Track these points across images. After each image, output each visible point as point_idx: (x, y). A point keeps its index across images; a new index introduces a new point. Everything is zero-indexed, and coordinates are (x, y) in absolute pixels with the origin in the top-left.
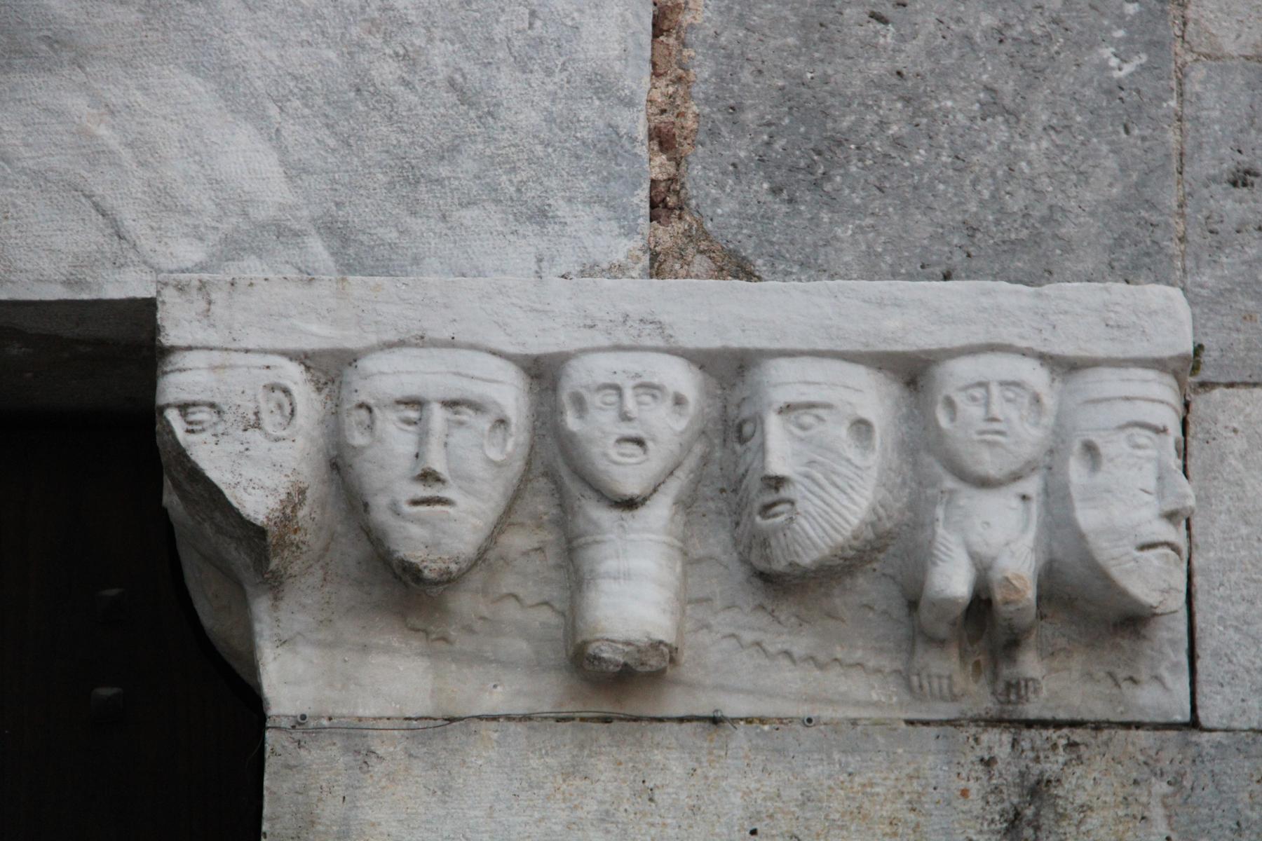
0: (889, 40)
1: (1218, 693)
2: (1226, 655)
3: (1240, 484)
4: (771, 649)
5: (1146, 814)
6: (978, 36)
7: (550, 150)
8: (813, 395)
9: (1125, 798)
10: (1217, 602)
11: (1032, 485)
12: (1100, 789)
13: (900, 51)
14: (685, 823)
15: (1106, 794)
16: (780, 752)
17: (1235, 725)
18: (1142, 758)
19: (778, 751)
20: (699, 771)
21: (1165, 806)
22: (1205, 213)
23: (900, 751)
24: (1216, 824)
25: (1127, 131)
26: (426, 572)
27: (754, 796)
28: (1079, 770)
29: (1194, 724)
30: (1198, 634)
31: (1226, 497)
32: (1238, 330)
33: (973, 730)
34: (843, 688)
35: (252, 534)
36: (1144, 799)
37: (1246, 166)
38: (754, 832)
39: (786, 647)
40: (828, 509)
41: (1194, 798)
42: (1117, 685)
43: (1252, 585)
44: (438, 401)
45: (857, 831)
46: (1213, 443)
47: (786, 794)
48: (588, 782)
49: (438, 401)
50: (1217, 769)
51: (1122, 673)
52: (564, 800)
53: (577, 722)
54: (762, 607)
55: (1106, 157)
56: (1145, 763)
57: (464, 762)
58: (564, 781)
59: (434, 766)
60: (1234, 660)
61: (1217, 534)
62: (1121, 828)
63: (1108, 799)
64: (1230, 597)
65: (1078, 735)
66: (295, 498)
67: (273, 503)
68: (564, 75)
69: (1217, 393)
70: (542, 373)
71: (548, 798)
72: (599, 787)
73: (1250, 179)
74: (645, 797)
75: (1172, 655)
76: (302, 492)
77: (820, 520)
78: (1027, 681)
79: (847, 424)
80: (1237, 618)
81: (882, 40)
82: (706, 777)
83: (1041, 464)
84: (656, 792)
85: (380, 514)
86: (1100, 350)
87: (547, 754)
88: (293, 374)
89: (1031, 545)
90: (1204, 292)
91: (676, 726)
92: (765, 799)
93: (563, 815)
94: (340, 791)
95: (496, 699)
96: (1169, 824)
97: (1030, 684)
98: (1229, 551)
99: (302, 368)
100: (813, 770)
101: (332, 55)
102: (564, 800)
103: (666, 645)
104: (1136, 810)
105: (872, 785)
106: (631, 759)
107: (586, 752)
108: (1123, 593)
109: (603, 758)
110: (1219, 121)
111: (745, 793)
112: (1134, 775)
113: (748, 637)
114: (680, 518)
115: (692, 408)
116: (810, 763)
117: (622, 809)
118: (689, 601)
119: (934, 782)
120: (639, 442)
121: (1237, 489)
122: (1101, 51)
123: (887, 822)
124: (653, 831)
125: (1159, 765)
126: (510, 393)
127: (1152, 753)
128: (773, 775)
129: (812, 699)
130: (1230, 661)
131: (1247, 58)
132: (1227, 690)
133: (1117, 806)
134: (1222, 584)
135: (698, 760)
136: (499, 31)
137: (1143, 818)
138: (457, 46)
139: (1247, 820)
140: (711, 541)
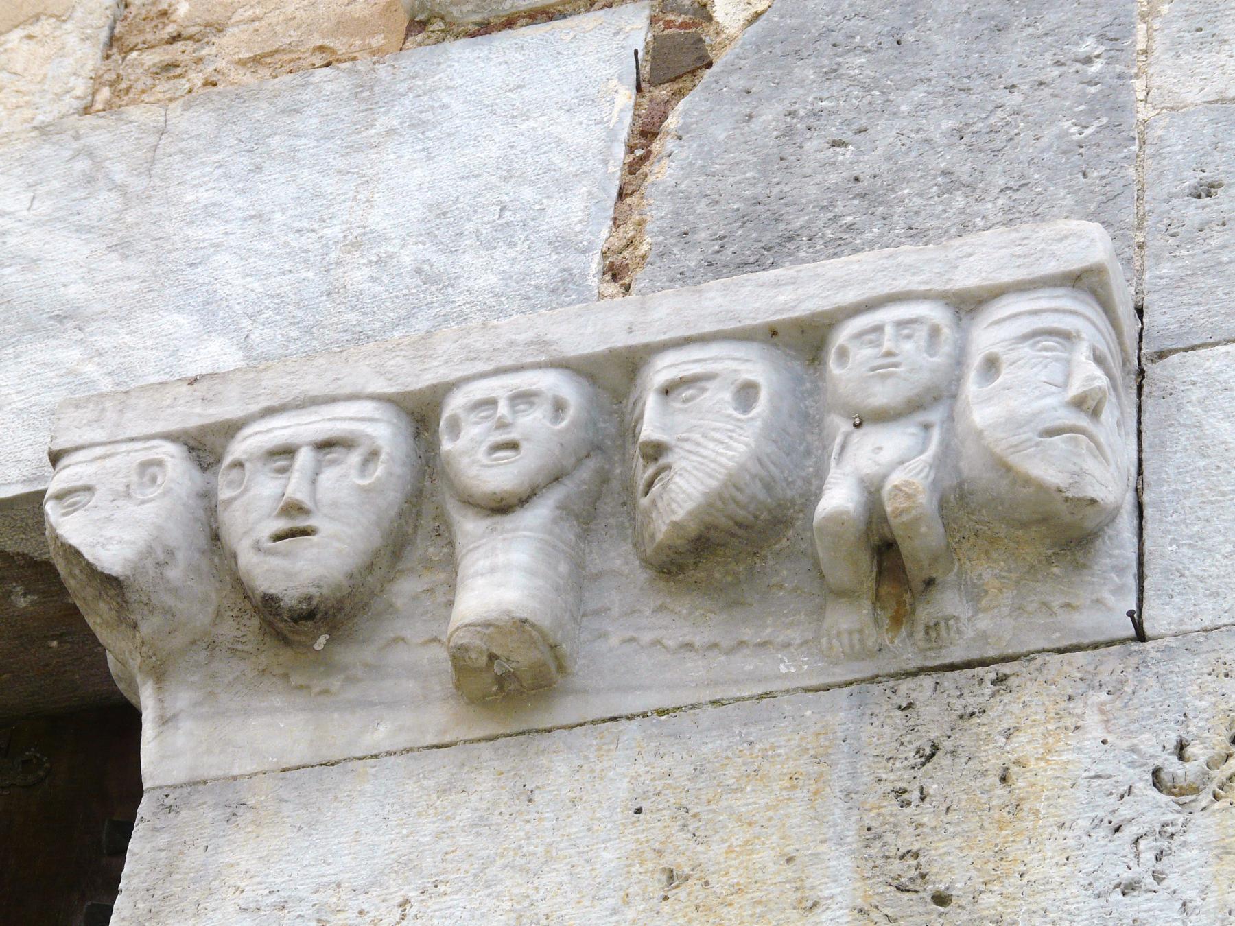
0: (848, 156)
1: (1167, 604)
2: (1178, 570)
3: (1199, 426)
4: (671, 643)
5: (1080, 723)
6: (937, 137)
7: (503, 299)
8: (696, 369)
9: (1057, 714)
10: (1169, 527)
11: (935, 416)
12: (1028, 711)
13: (858, 162)
14: (563, 815)
15: (1036, 713)
16: (677, 736)
17: (1184, 628)
18: (1078, 675)
19: (674, 735)
20: (585, 767)
21: (1102, 712)
22: (1166, 222)
23: (808, 713)
24: (1160, 719)
25: (1085, 176)
26: (286, 599)
27: (642, 779)
28: (1007, 698)
29: (1141, 636)
30: (1146, 558)
31: (1183, 439)
32: (1198, 304)
33: (892, 683)
34: (748, 668)
35: (111, 585)
36: (1078, 711)
37: (1210, 180)
38: (639, 811)
39: (688, 639)
40: (705, 461)
41: (1136, 701)
42: (1053, 614)
43: (1209, 507)
44: (308, 444)
45: (753, 790)
46: (1170, 399)
47: (675, 772)
48: (464, 794)
49: (308, 444)
50: (1162, 670)
51: (1056, 602)
52: (436, 814)
53: (461, 745)
54: (661, 608)
55: (1064, 198)
56: (1082, 679)
57: (336, 797)
58: (439, 798)
59: (305, 806)
60: (1187, 573)
61: (1171, 470)
62: (1051, 740)
63: (1038, 718)
64: (1183, 521)
65: (1005, 669)
66: (158, 556)
67: (129, 553)
68: (526, 244)
69: (1174, 358)
70: (421, 414)
71: (419, 815)
72: (473, 798)
73: (1213, 190)
74: (523, 798)
75: (1116, 579)
76: (170, 553)
77: (695, 472)
78: (947, 619)
79: (733, 388)
80: (1191, 537)
81: (841, 158)
82: (592, 771)
83: (946, 394)
84: (536, 792)
85: (248, 560)
86: (1005, 277)
87: (424, 777)
88: (171, 453)
89: (930, 460)
90: (1164, 282)
91: (566, 732)
92: (654, 780)
93: (431, 828)
94: (202, 843)
95: (381, 735)
96: (1106, 728)
97: (951, 622)
98: (1185, 483)
99: (185, 448)
100: (710, 746)
101: (310, 275)
102: (436, 814)
103: (533, 625)
104: (1069, 722)
105: (773, 748)
106: (514, 768)
107: (466, 769)
108: (1027, 481)
109: (484, 771)
110: (1181, 152)
111: (632, 777)
112: (1070, 691)
113: (646, 637)
114: (569, 532)
115: (571, 413)
116: (707, 740)
117: (497, 812)
118: (580, 580)
119: (841, 735)
120: (513, 446)
121: (1195, 430)
122: (1061, 124)
123: (787, 778)
124: (528, 826)
125: (1099, 678)
126: (384, 431)
127: (1091, 668)
128: (666, 758)
129: (715, 683)
130: (1182, 575)
131: (1210, 102)
132: (1177, 600)
133: (1047, 721)
134: (1175, 511)
135: (586, 758)
136: (469, 227)
137: (1077, 728)
138: (428, 244)
139: (1195, 709)
140: (612, 554)
